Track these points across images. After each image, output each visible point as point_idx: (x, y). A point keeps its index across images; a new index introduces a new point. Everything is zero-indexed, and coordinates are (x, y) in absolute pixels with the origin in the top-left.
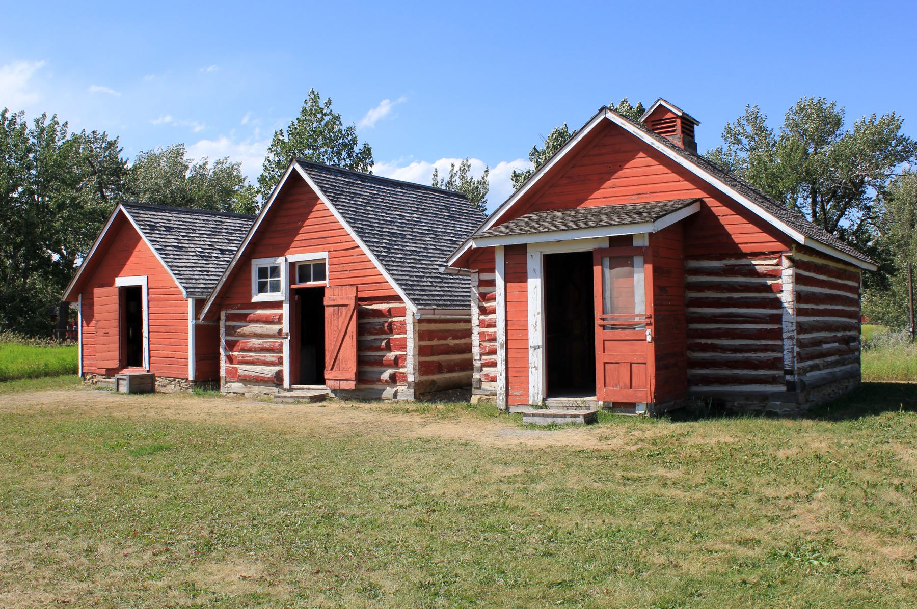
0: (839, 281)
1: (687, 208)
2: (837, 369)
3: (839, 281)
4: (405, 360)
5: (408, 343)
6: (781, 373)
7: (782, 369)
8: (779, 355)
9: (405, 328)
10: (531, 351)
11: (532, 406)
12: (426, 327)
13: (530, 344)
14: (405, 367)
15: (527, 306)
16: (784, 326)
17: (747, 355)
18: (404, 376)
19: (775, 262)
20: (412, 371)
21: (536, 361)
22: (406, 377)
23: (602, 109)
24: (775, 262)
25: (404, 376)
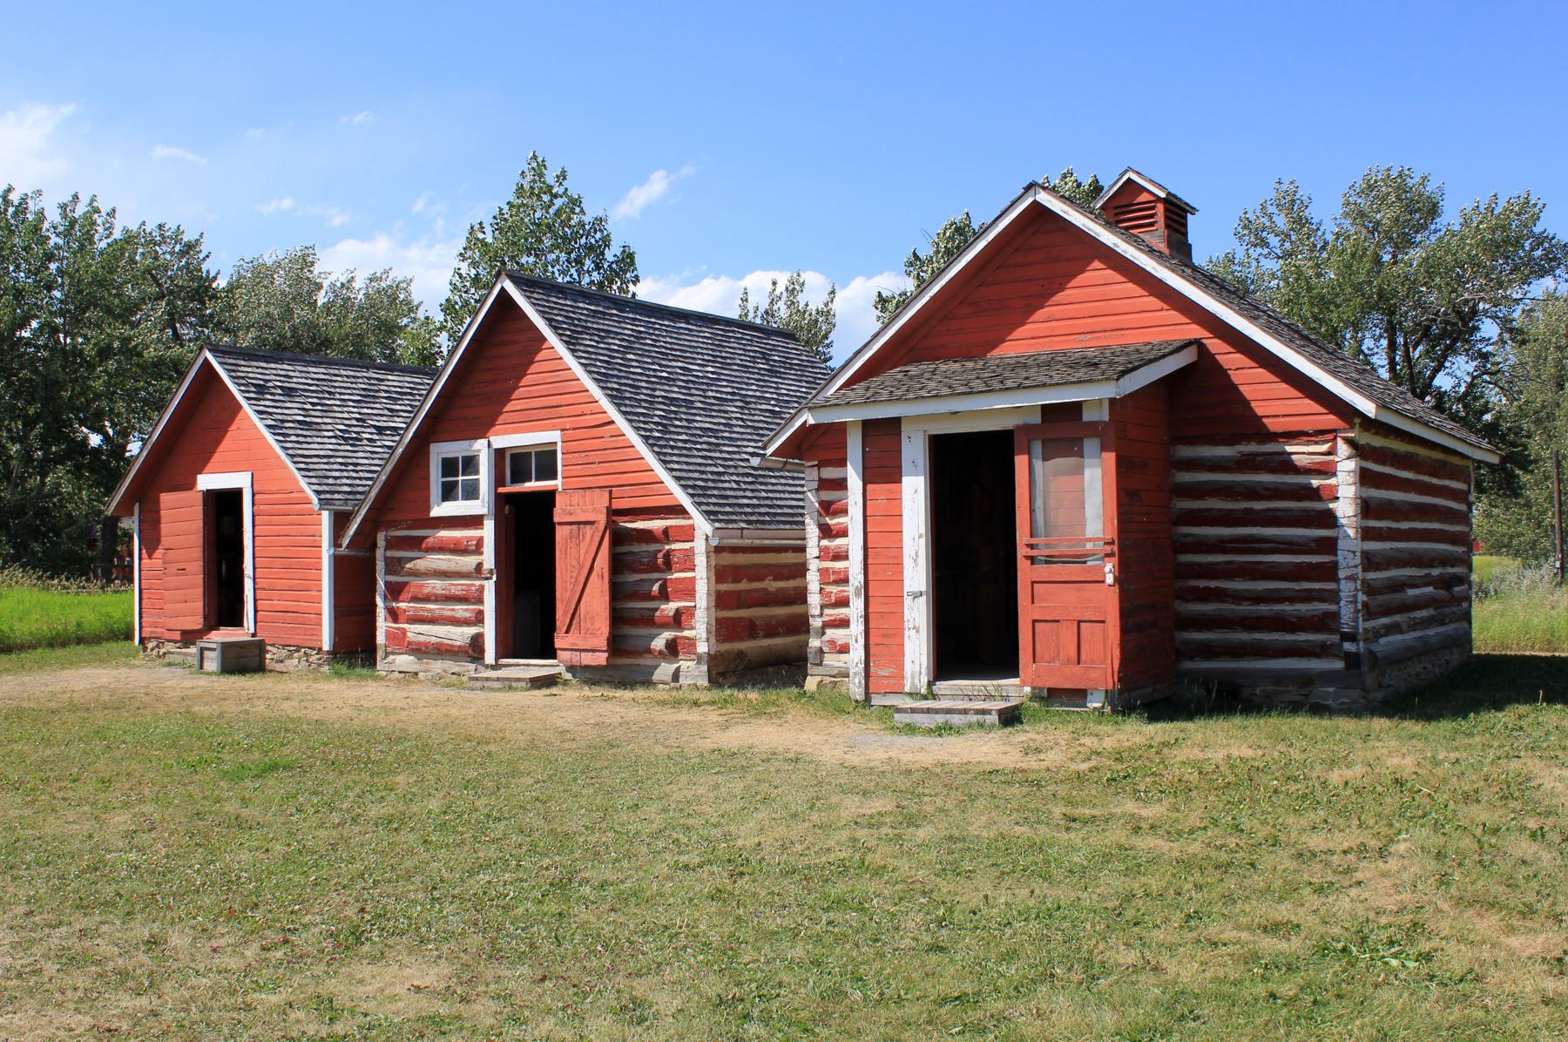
0: (1435, 481)
1: (1175, 356)
2: (1431, 632)
3: (1435, 481)
4: (693, 615)
5: (698, 587)
6: (1336, 638)
7: (1337, 631)
8: (1333, 607)
9: (693, 561)
10: (907, 601)
11: (910, 694)
12: (728, 559)
13: (907, 588)
14: (692, 628)
15: (901, 523)
16: (1340, 558)
17: (1277, 607)
18: (692, 643)
19: (1325, 448)
20: (704, 636)
21: (917, 617)
22: (694, 645)
23: (1030, 187)
24: (1325, 448)
25: (692, 643)
